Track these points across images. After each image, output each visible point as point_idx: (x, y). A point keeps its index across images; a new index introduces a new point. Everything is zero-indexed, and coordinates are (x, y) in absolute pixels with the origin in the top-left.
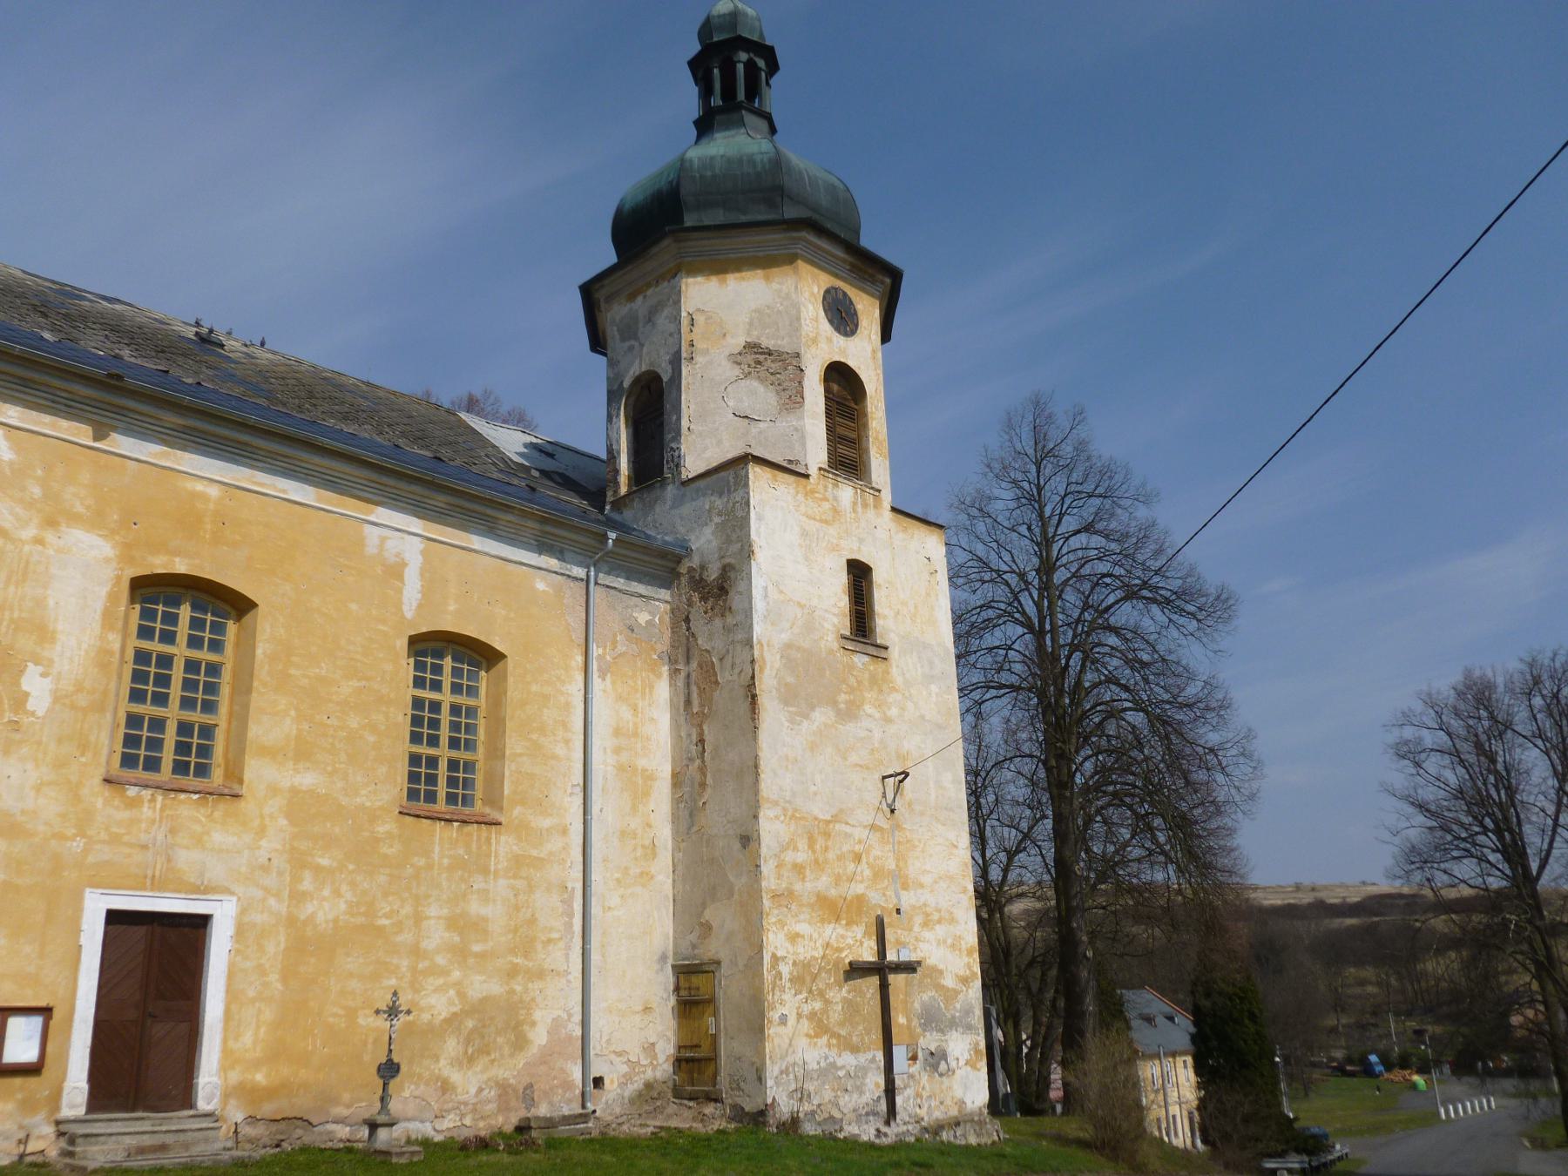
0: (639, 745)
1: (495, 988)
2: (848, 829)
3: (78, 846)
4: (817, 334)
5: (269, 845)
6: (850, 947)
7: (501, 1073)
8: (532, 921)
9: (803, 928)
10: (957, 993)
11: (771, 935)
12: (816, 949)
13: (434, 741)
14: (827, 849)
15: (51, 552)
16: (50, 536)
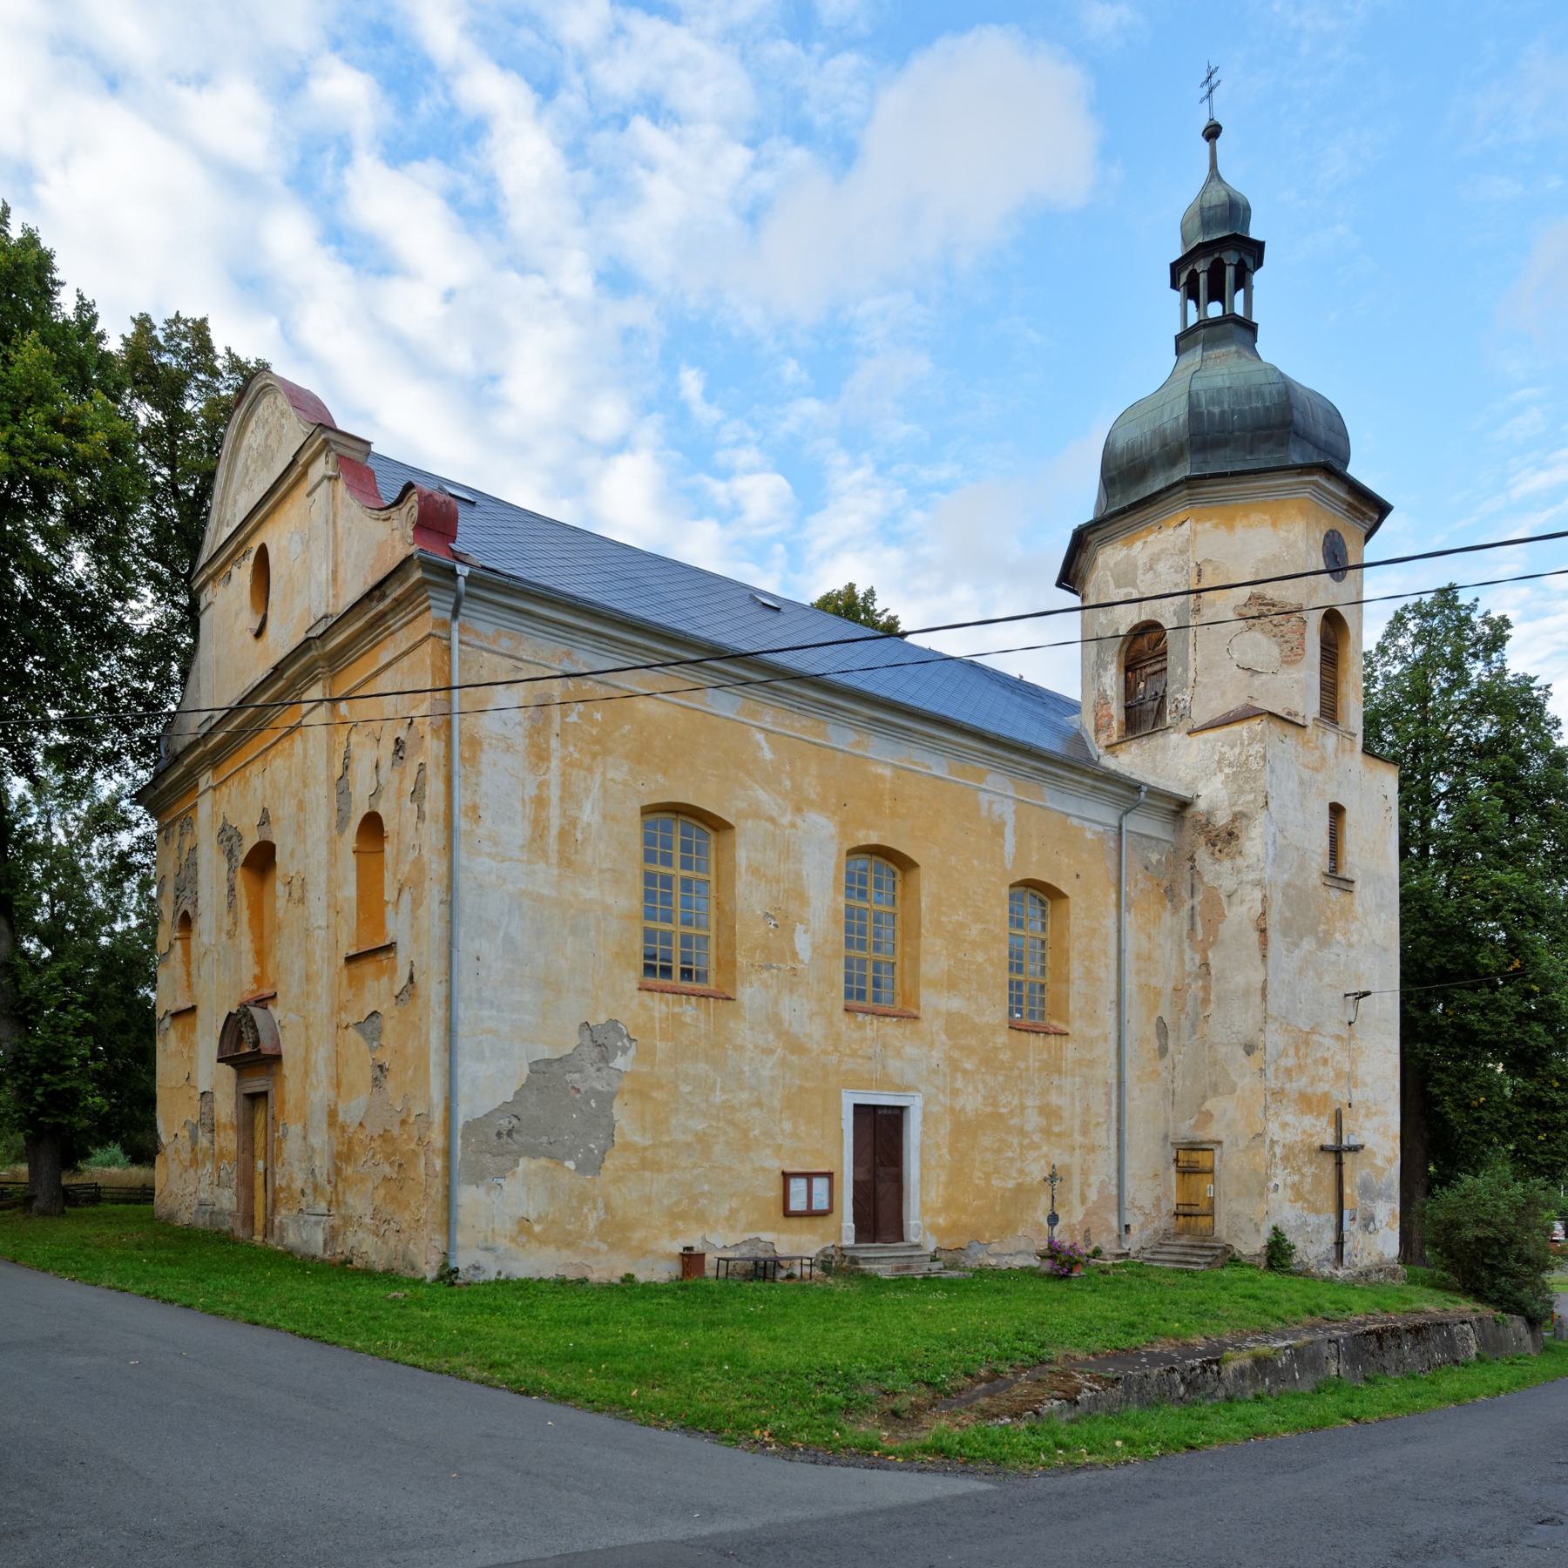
5: (936, 1054)
6: (1318, 1133)
9: (1289, 1118)
10: (1384, 1170)
14: (1306, 1056)
15: (800, 833)
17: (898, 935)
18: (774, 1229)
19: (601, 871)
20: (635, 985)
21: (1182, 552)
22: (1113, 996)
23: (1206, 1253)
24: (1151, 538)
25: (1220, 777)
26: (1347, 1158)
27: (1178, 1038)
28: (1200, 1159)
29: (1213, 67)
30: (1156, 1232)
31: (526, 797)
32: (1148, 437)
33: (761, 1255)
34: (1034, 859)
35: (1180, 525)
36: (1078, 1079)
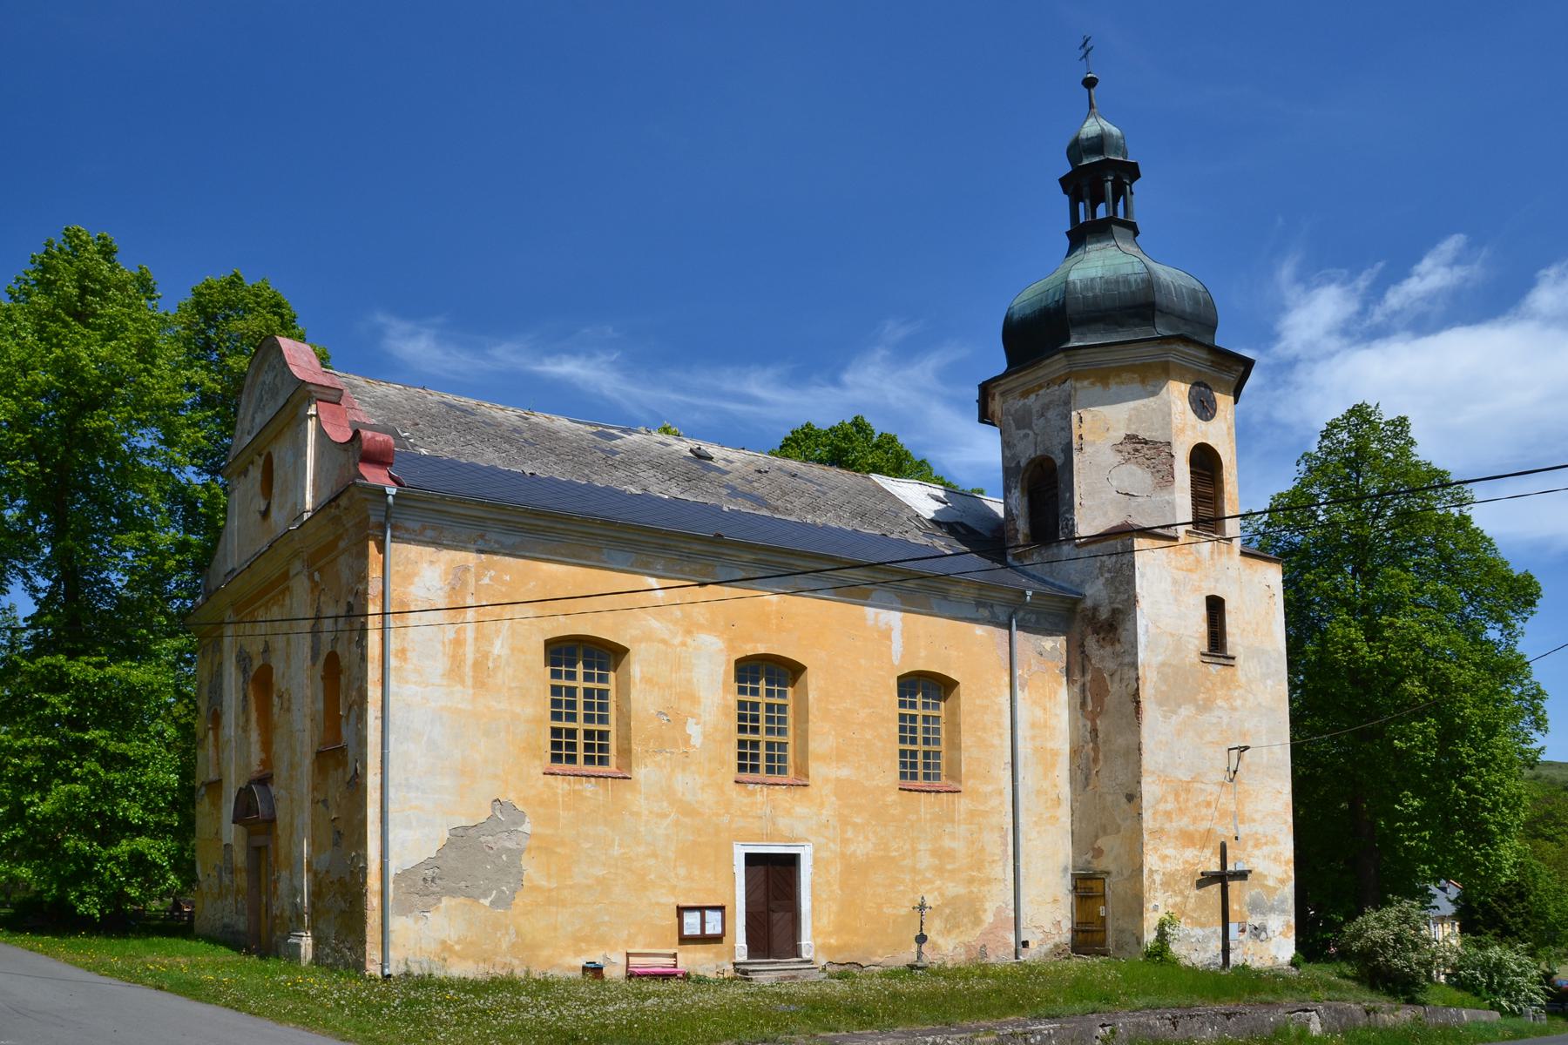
0: (1048, 734)
1: (961, 890)
2: (1203, 786)
4: (1185, 424)
5: (826, 813)
7: (966, 939)
8: (983, 849)
9: (1170, 852)
10: (1276, 889)
11: (1148, 857)
12: (1178, 864)
13: (913, 741)
14: (1188, 800)
16: (689, 641)
19: (510, 689)
20: (540, 771)
25: (1102, 580)
26: (1234, 886)
31: (446, 640)
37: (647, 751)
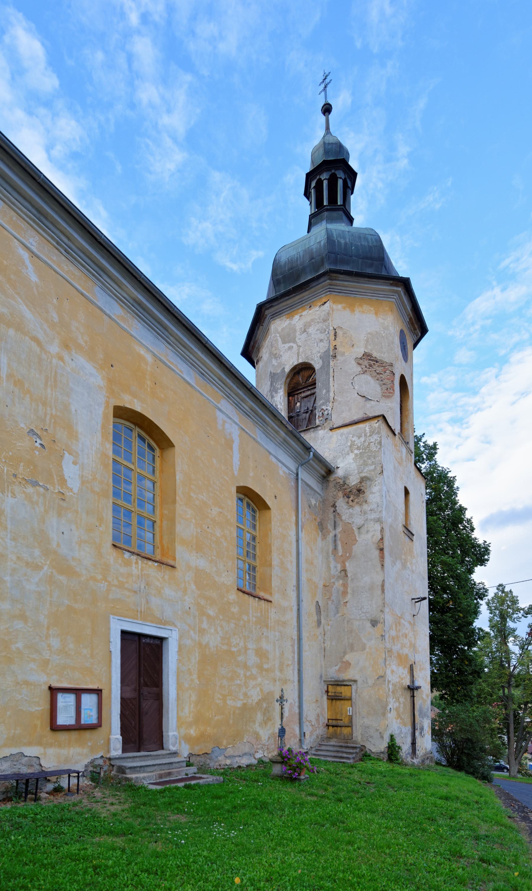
3: (104, 586)
17: (158, 500)
18: (40, 743)
21: (325, 321)
22: (294, 582)
23: (351, 751)
24: (304, 313)
25: (352, 456)
27: (327, 616)
28: (343, 691)
29: (327, 73)
30: (317, 737)
32: (301, 254)
33: (25, 770)
34: (251, 474)
35: (323, 304)
36: (277, 634)
37: (15, 476)
